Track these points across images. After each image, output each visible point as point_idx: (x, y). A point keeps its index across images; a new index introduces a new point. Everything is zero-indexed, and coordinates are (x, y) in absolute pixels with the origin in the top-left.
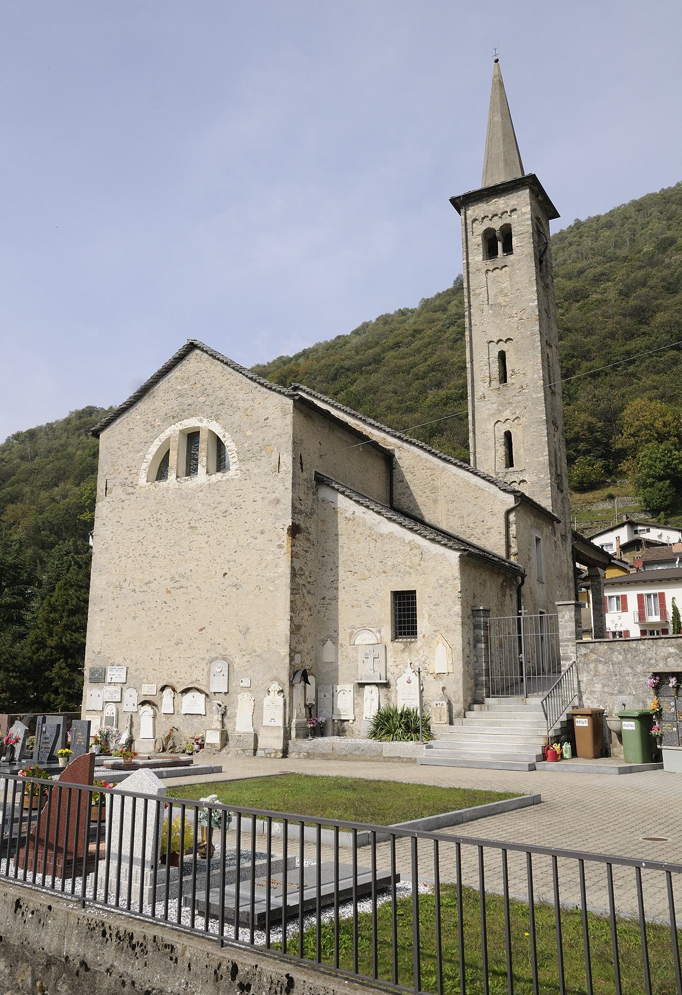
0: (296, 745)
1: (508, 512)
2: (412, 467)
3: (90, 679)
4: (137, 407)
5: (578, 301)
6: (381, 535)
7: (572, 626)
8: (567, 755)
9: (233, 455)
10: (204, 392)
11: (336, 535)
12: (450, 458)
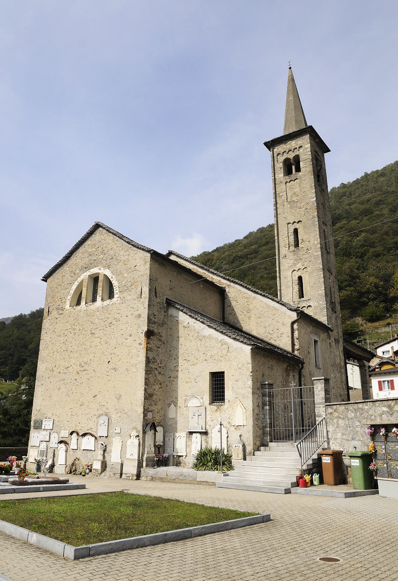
0: (145, 472)
1: (293, 323)
2: (236, 297)
3: (34, 426)
4: (67, 263)
5: (366, 216)
6: (204, 337)
7: (322, 394)
8: (316, 483)
9: (116, 289)
10: (103, 253)
11: (178, 337)
12: (258, 290)
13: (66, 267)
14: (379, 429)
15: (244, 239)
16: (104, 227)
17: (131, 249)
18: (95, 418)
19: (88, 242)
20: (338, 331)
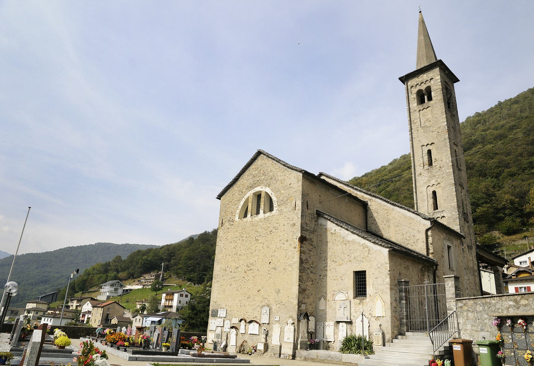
0: (299, 353)
1: (427, 230)
3: (211, 315)
5: (500, 140)
6: (349, 241)
7: (453, 290)
9: (275, 203)
12: (395, 203)
13: (235, 188)
14: (506, 320)
15: (389, 165)
16: (265, 153)
17: (287, 170)
18: (259, 309)
19: (253, 166)
20: (471, 239)
